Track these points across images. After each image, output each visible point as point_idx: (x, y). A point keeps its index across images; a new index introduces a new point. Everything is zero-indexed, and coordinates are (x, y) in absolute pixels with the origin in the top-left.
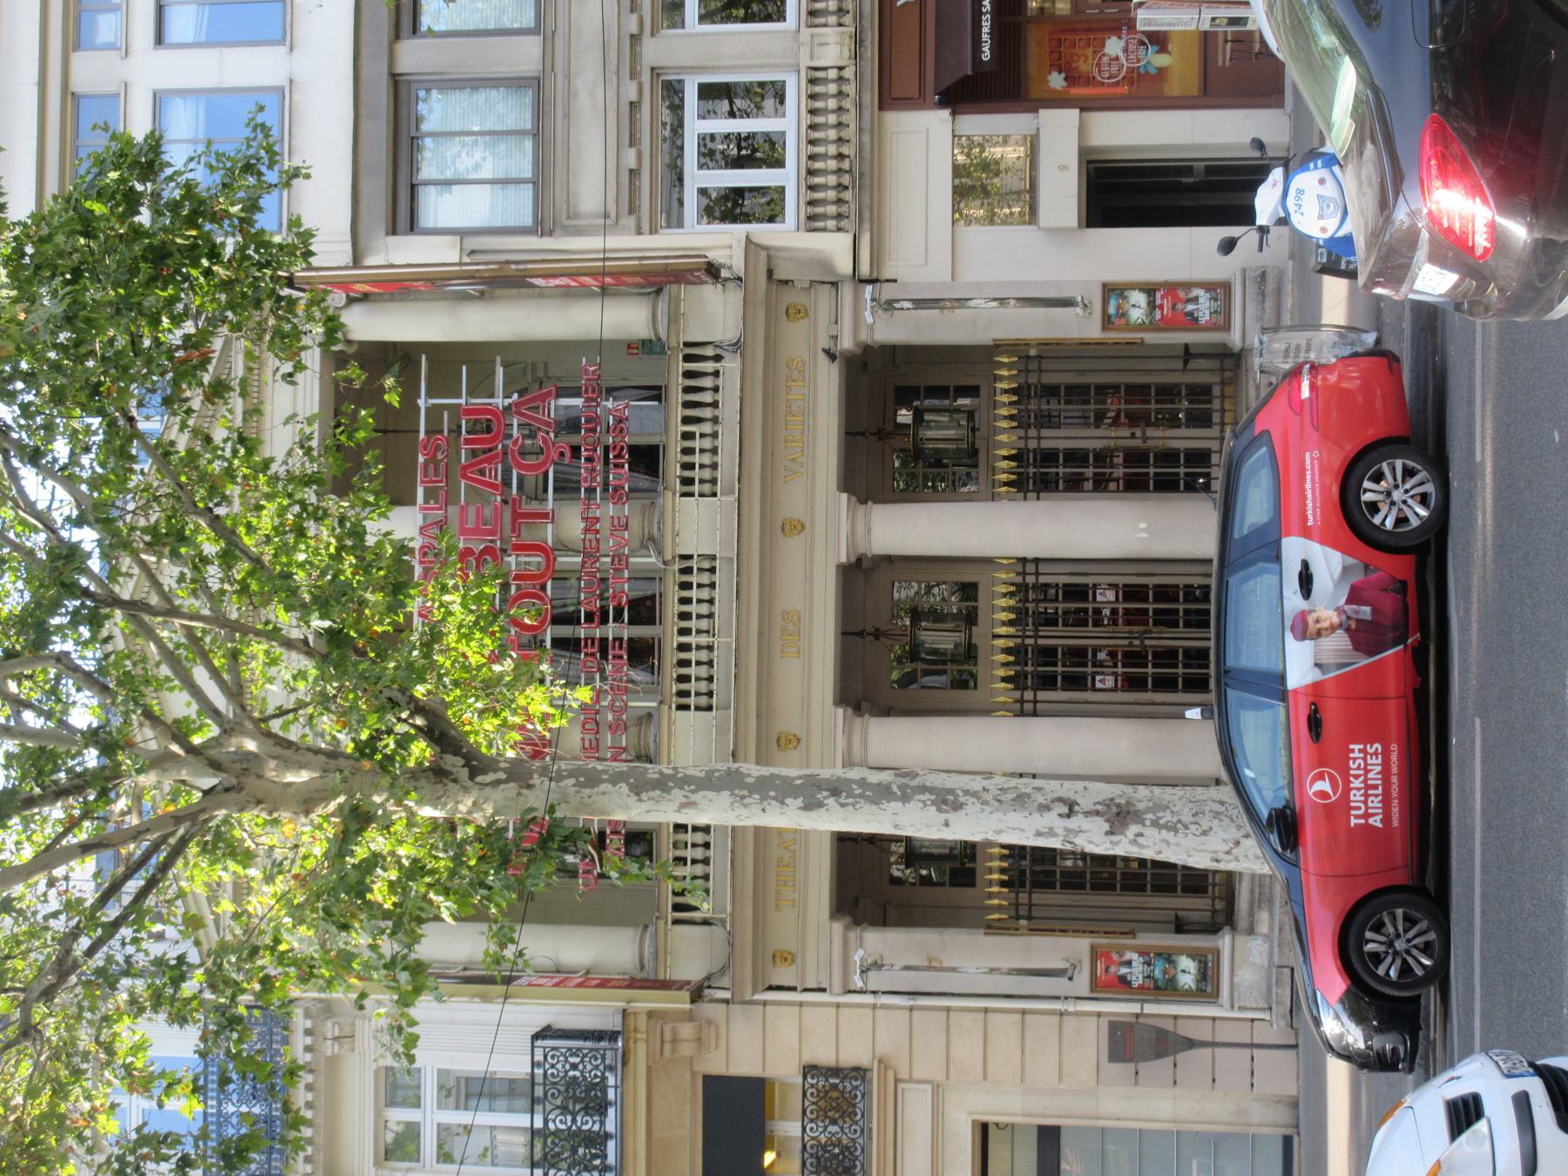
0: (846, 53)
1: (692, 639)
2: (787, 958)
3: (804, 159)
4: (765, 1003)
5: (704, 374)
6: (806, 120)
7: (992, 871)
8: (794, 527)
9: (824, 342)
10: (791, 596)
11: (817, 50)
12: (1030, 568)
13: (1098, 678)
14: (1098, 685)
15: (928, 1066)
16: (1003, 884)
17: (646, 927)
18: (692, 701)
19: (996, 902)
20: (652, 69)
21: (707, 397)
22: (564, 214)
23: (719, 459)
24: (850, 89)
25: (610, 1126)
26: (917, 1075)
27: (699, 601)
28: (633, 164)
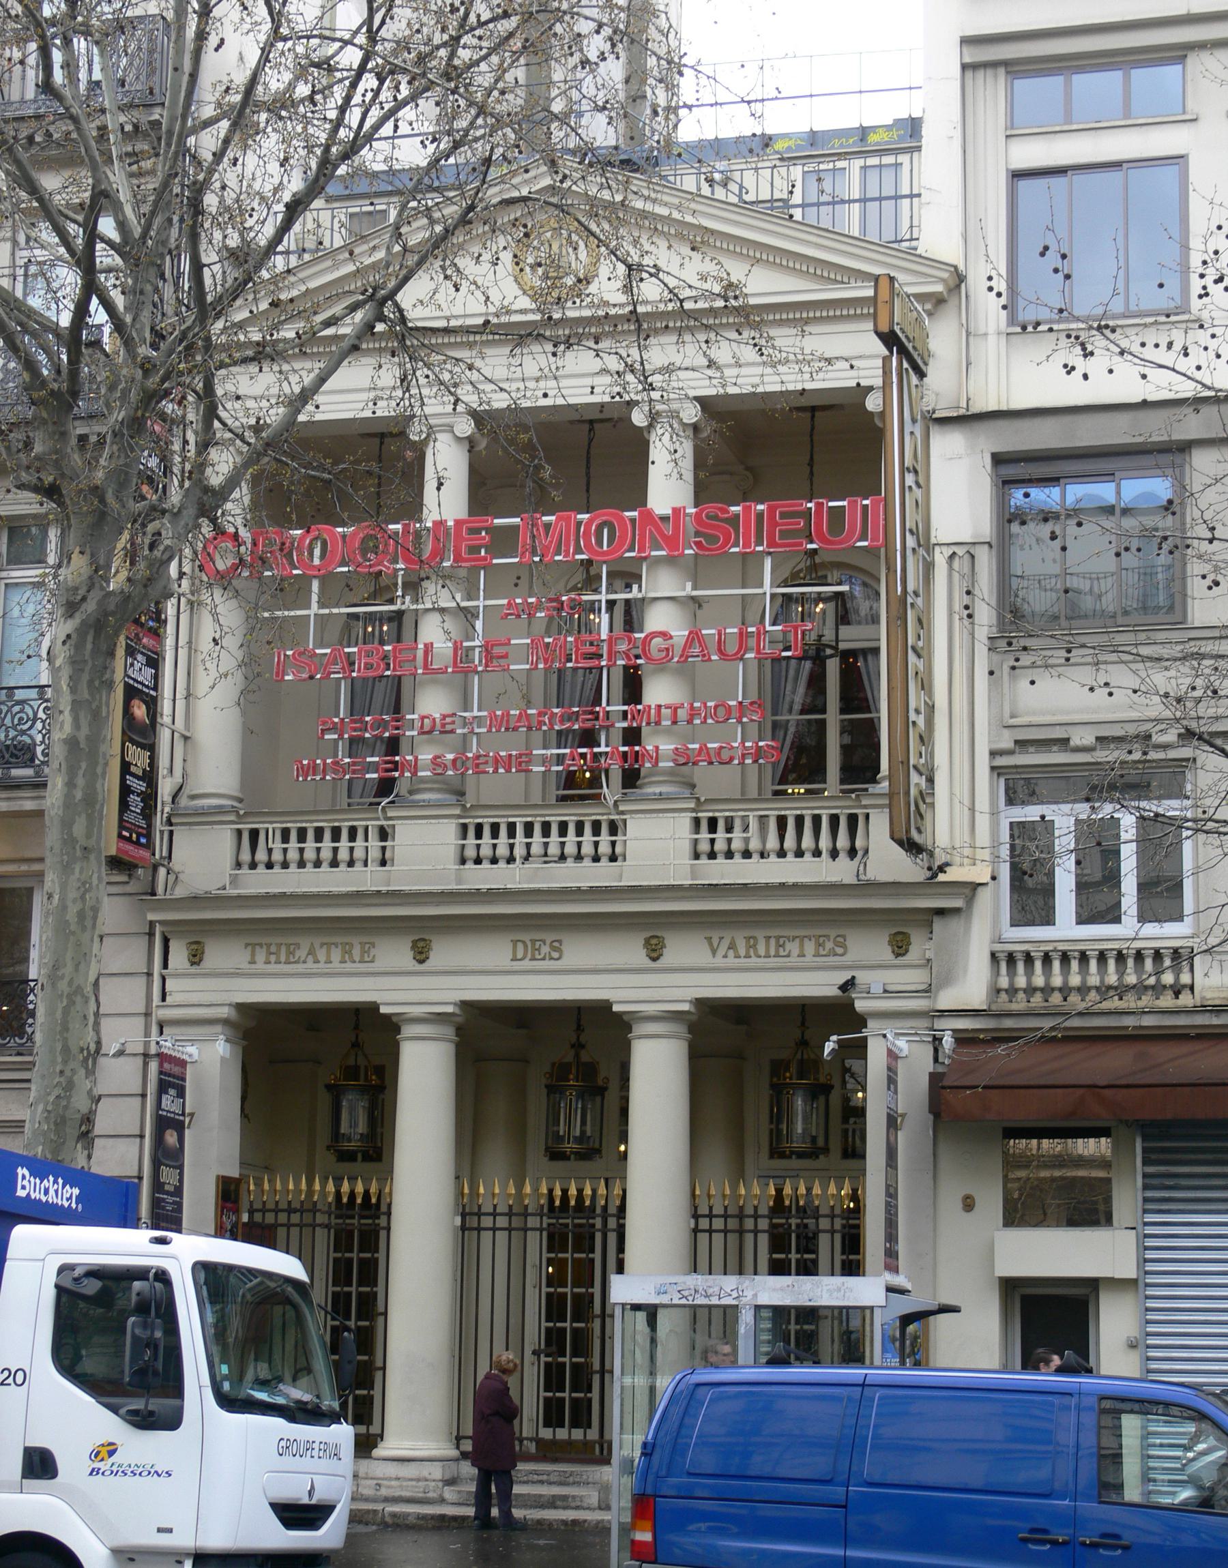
0: (1209, 995)
1: (520, 838)
2: (196, 958)
6: (1092, 949)
7: (583, 1185)
8: (655, 951)
9: (862, 977)
10: (581, 951)
12: (704, 1223)
17: (240, 800)
19: (317, 1187)
24: (1037, 999)
27: (579, 844)
28: (1076, 741)
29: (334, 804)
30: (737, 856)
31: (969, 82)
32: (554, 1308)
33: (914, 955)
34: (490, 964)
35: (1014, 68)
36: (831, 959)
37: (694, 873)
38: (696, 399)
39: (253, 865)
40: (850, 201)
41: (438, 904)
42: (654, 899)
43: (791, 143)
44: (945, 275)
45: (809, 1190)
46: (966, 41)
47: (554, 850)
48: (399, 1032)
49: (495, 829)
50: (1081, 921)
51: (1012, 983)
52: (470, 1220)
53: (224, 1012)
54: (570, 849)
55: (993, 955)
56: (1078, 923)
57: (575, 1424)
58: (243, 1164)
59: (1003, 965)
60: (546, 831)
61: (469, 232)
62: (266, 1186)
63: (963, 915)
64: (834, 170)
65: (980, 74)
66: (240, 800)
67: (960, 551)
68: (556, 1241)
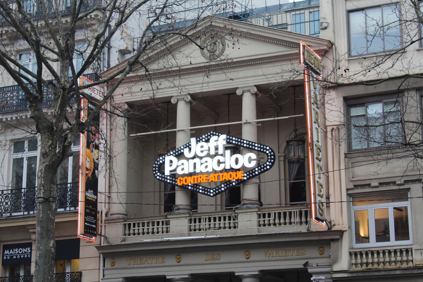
2: (113, 264)
5: (280, 220)
9: (310, 261)
10: (225, 257)
11: (419, 251)
18: (262, 219)
20: (410, 189)
23: (267, 227)
24: (399, 265)
29: (160, 213)
33: (325, 255)
34: (170, 264)
36: (300, 256)
38: (255, 86)
39: (129, 235)
41: (182, 244)
43: (288, 6)
44: (327, 43)
47: (217, 226)
50: (377, 241)
51: (356, 262)
54: (222, 225)
56: (376, 242)
59: (353, 256)
61: (129, 62)
63: (340, 240)
66: (126, 215)
67: (335, 127)
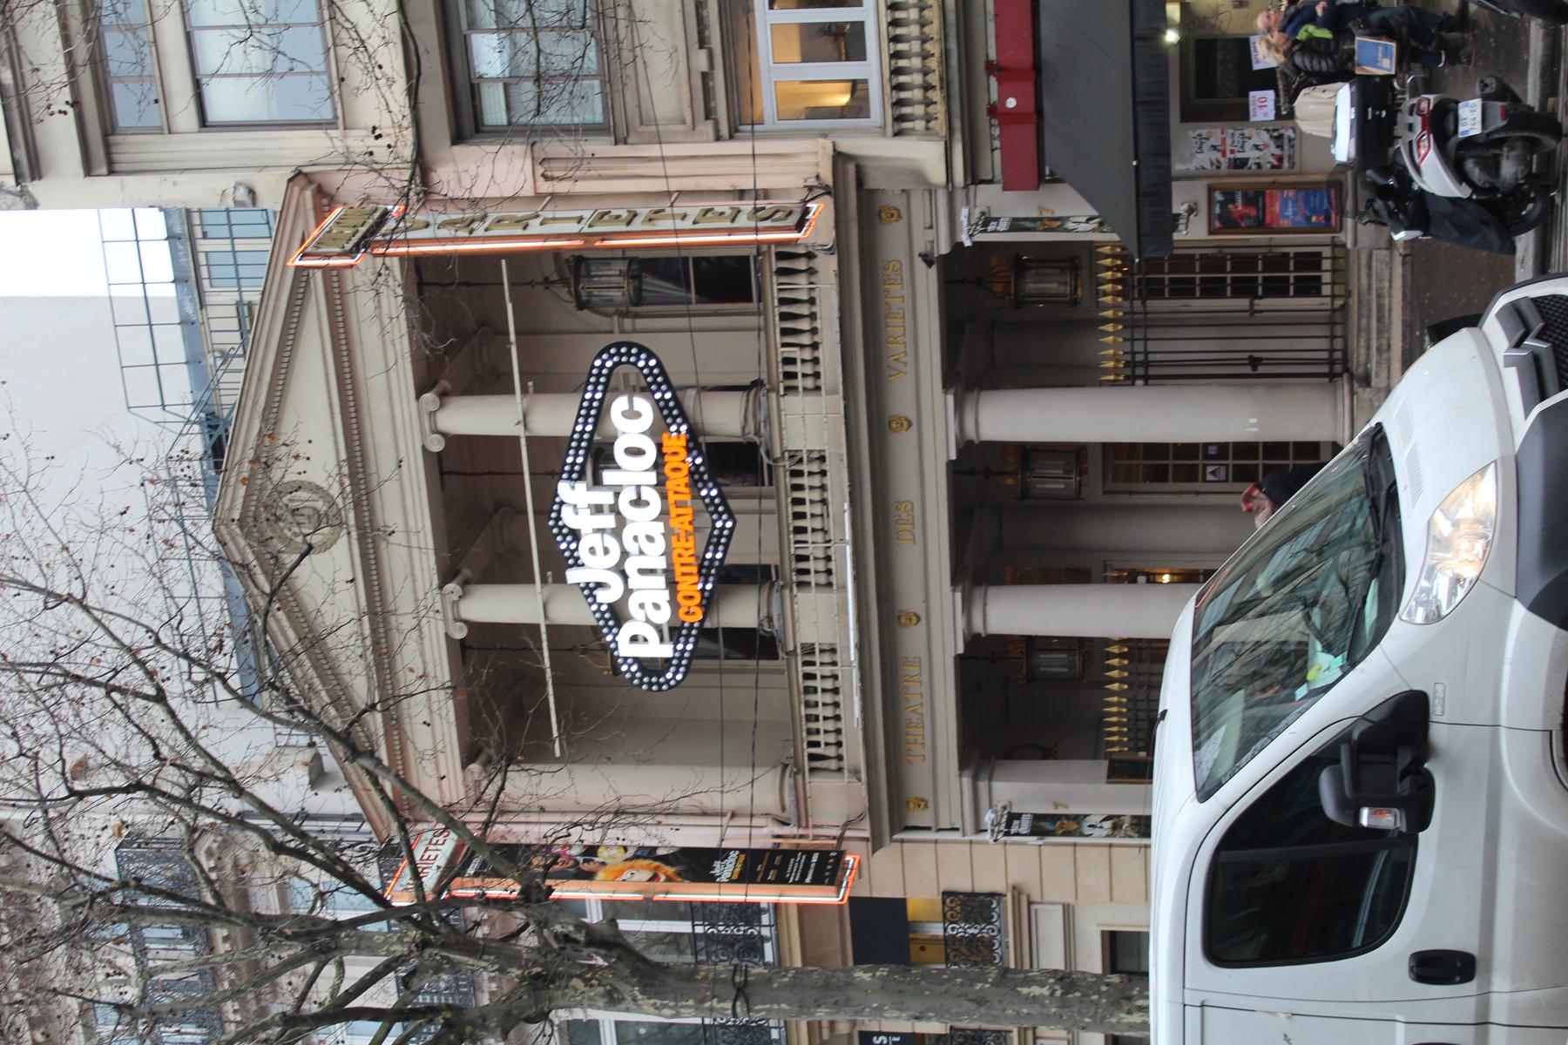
3: (886, 58)
4: (902, 841)
6: (886, 16)
9: (920, 247)
10: (905, 486)
13: (1210, 469)
14: (1210, 477)
15: (1057, 890)
16: (1116, 294)
21: (805, 339)
22: (637, 121)
25: (765, 932)
26: (1047, 898)
28: (704, 67)
30: (814, 309)
31: (124, 167)
32: (1213, 289)
33: (899, 203)
35: (109, 129)
37: (833, 392)
39: (840, 758)
40: (240, 292)
41: (868, 609)
42: (858, 440)
44: (296, 190)
45: (1108, 269)
46: (88, 170)
47: (818, 509)
48: (972, 442)
49: (808, 690)
52: (1140, 372)
53: (967, 781)
54: (816, 495)
55: (897, 134)
57: (1318, 267)
58: (1095, 757)
60: (801, 516)
62: (1115, 738)
63: (861, 162)
64: (208, 265)
65: (117, 157)
67: (540, 170)
68: (1153, 290)
